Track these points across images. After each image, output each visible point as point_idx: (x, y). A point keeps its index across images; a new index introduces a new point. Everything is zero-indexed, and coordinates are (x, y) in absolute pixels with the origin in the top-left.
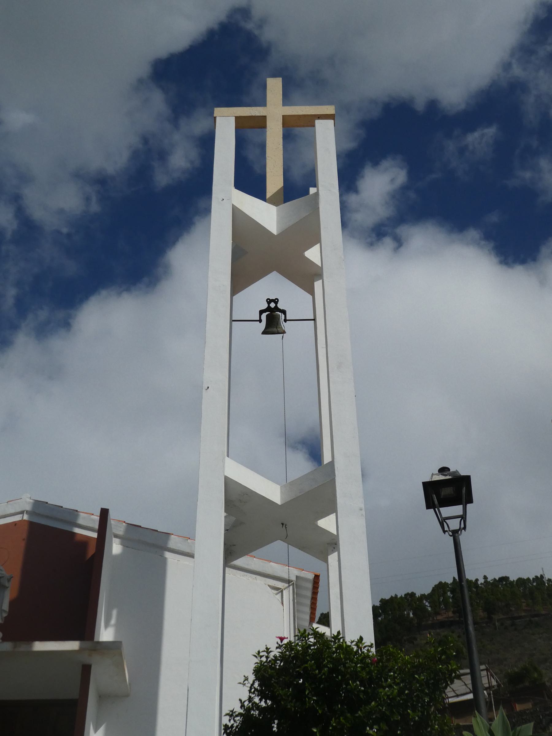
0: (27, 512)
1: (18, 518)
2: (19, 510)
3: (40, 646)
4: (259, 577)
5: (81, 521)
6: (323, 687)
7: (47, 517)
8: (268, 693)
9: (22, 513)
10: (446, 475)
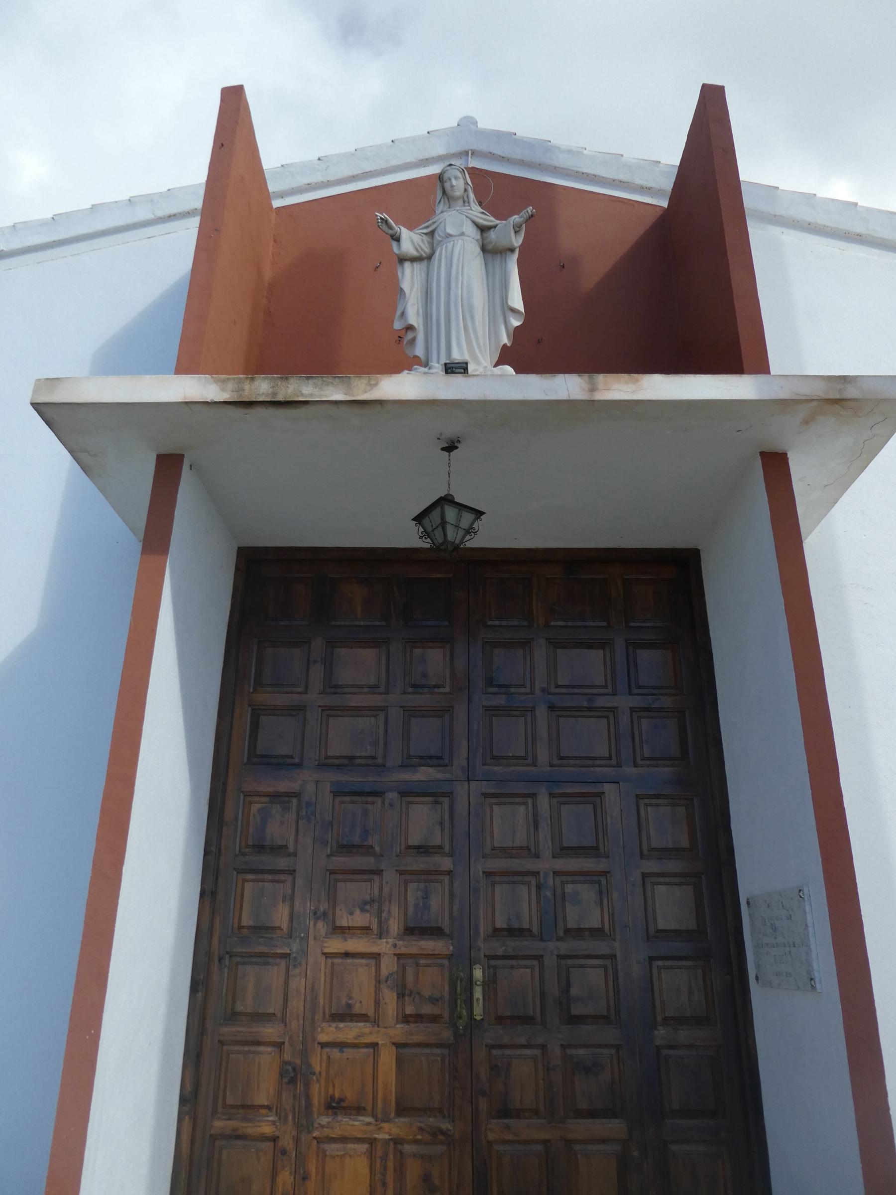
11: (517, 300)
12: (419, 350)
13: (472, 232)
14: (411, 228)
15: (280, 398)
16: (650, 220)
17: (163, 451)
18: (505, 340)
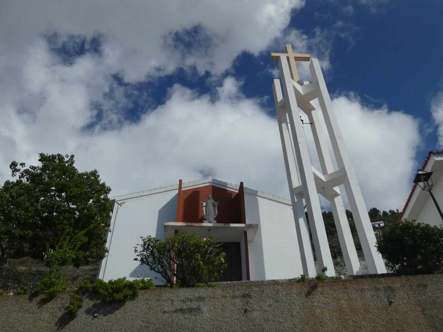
0: (211, 182)
1: (208, 184)
2: (208, 182)
3: (232, 225)
4: (287, 206)
5: (228, 186)
6: (46, 216)
7: (218, 184)
8: (62, 218)
9: (209, 183)
10: (423, 172)
11: (217, 212)
12: (205, 218)
13: (212, 203)
14: (204, 202)
15: (192, 225)
16: (236, 194)
17: (176, 230)
18: (215, 217)
